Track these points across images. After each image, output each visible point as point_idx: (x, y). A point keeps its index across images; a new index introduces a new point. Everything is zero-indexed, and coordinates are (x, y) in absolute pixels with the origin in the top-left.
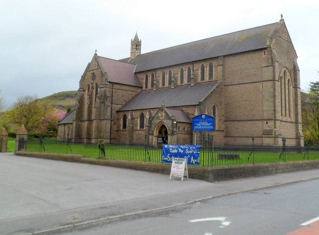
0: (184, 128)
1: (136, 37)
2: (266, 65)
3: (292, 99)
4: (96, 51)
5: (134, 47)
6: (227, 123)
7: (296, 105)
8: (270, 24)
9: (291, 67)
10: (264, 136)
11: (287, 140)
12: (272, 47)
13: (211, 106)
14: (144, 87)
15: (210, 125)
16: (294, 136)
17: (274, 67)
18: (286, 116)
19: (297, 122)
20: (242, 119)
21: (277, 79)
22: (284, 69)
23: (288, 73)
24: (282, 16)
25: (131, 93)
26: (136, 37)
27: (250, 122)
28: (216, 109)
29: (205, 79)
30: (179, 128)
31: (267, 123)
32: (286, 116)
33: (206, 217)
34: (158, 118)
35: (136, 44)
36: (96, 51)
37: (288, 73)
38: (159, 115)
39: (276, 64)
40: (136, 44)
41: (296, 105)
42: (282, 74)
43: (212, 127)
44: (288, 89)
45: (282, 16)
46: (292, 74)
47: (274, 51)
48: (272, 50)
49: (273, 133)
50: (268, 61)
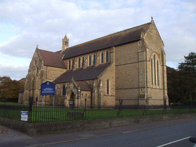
0: (87, 95)
1: (66, 37)
2: (140, 51)
3: (160, 74)
4: (37, 46)
5: (65, 43)
6: (117, 90)
7: (163, 77)
8: (142, 25)
9: (160, 52)
10: (139, 99)
11: (123, 101)
12: (144, 38)
13: (106, 80)
14: (68, 68)
15: (52, 90)
16: (162, 98)
17: (146, 51)
18: (155, 85)
19: (164, 89)
20: (126, 88)
21: (148, 60)
22: (154, 54)
23: (157, 56)
24: (152, 18)
25: (59, 72)
26: (66, 37)
27: (131, 90)
28: (109, 81)
29: (104, 62)
30: (83, 94)
31: (142, 89)
32: (155, 85)
33: (167, 145)
34: (69, 88)
35: (66, 41)
36: (37, 46)
37: (157, 56)
38: (70, 86)
39: (148, 50)
40: (66, 41)
41: (163, 77)
42: (152, 57)
43: (53, 92)
44: (158, 67)
45: (152, 18)
46: (160, 56)
47: (146, 41)
48: (145, 40)
49: (145, 97)
50: (142, 48)
